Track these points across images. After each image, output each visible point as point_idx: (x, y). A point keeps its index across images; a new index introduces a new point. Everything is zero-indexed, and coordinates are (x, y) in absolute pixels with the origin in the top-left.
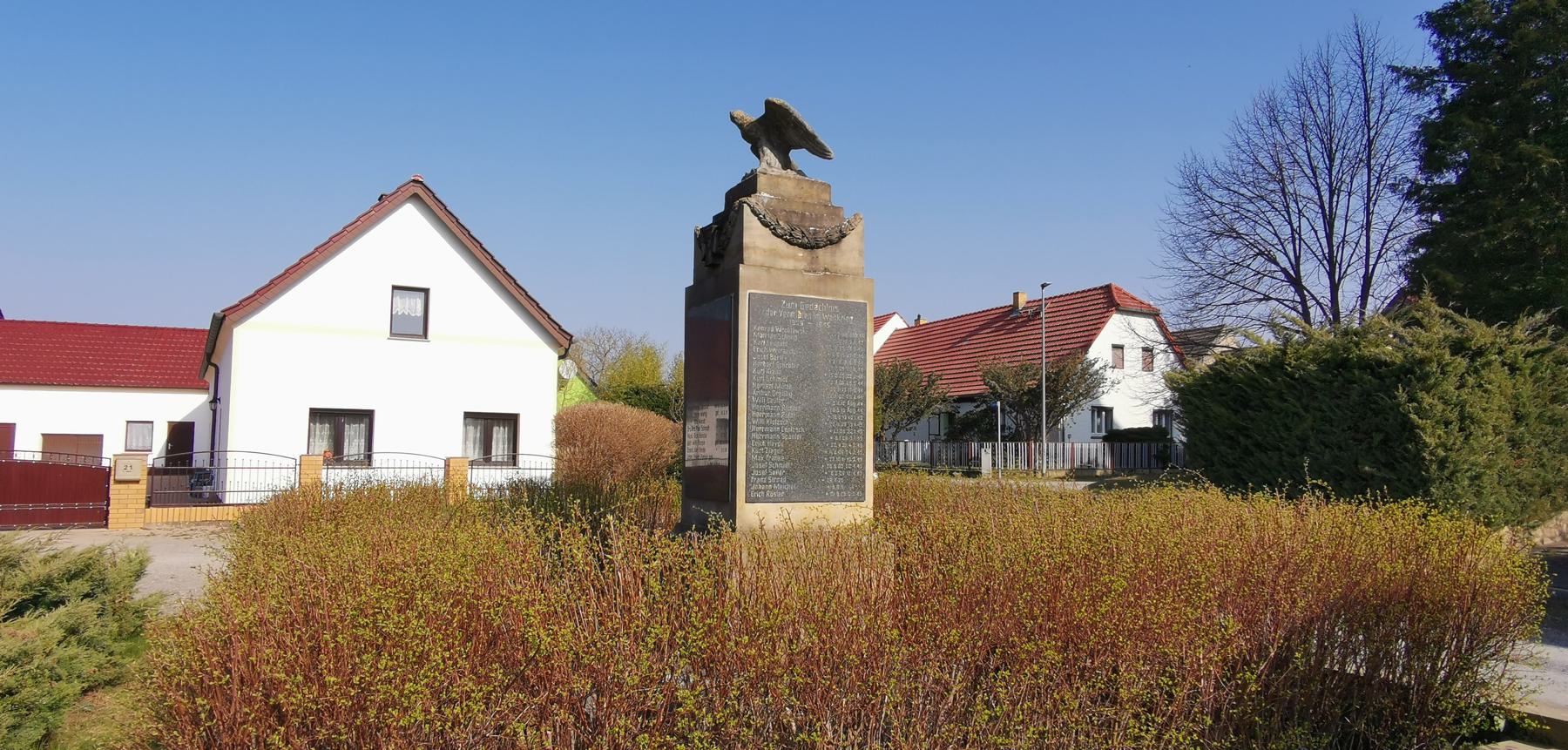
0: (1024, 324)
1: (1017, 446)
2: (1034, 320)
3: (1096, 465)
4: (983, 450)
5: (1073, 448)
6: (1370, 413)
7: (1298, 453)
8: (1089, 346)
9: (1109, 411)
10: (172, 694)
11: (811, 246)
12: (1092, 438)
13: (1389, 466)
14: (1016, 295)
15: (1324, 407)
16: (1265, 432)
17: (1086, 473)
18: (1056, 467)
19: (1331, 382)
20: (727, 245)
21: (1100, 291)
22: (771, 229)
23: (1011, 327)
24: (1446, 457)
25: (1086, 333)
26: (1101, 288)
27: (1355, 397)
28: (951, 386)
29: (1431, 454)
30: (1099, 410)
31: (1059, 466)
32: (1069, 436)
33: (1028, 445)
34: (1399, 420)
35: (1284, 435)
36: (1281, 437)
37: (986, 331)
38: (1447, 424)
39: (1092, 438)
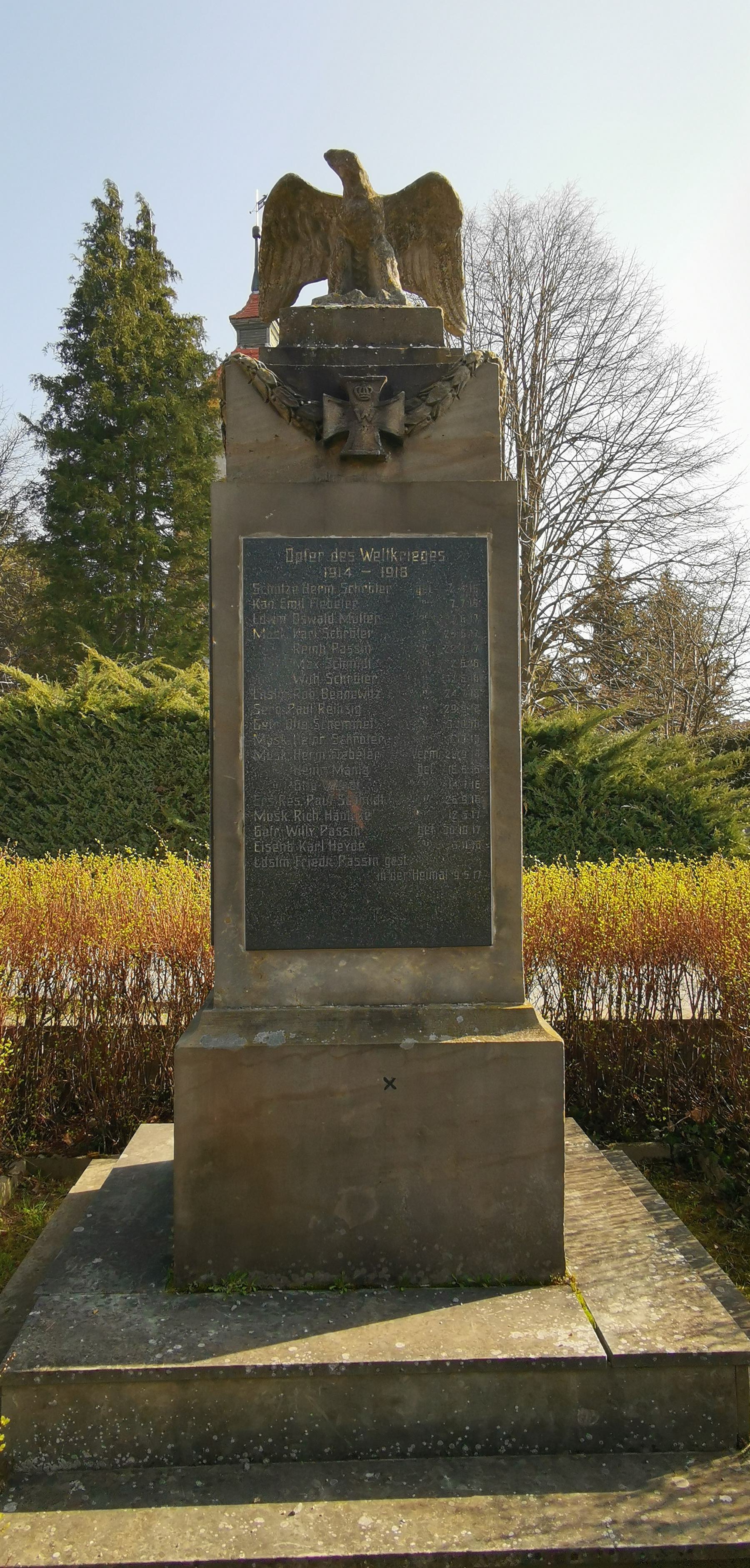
6: (173, 766)
13: (190, 818)
15: (127, 759)
20: (424, 429)
36: (67, 789)
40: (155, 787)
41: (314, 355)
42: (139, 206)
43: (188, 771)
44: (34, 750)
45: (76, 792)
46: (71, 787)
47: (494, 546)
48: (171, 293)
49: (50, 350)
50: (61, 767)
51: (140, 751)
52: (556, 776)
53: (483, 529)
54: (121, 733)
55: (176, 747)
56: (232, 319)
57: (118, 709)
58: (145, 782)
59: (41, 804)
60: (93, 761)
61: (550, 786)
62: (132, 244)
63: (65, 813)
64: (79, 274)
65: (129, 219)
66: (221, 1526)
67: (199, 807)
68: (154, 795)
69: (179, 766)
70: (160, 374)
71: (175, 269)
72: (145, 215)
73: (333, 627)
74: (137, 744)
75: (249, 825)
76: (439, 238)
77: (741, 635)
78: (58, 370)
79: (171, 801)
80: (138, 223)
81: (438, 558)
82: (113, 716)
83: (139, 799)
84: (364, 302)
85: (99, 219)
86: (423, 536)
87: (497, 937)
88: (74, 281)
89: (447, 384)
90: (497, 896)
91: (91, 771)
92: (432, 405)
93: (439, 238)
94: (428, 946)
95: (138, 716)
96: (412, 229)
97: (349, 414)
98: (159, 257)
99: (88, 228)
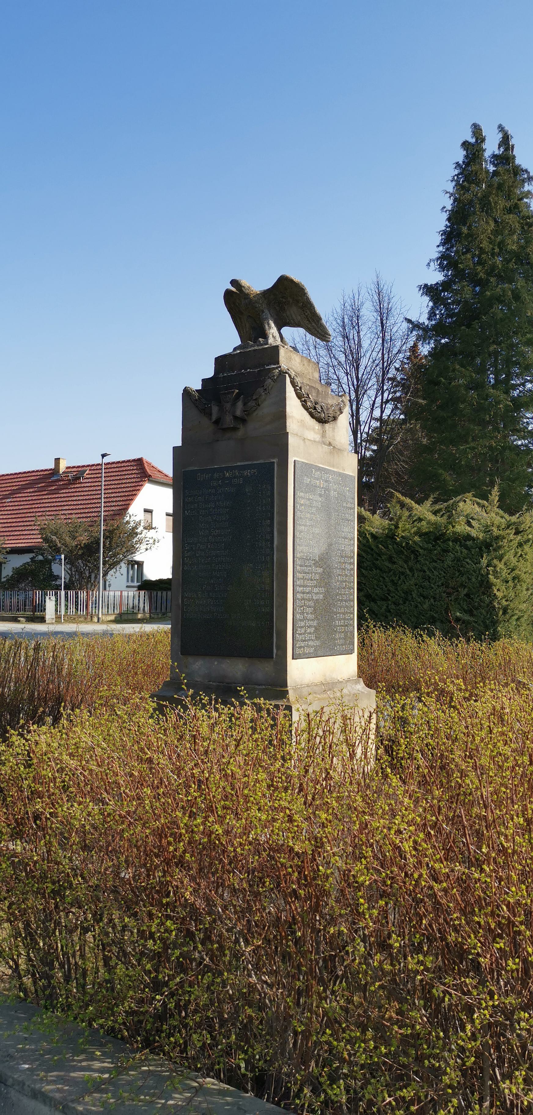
0: (65, 486)
1: (77, 594)
2: (74, 484)
3: (139, 610)
4: (47, 598)
5: (121, 596)
6: (457, 574)
7: (401, 602)
8: (127, 509)
9: (140, 565)
10: (425, 606)
11: (322, 421)
12: (127, 587)
13: (470, 612)
14: (57, 461)
15: (425, 568)
16: (376, 587)
17: (130, 617)
18: (108, 612)
19: (431, 550)
21: (133, 463)
23: (53, 488)
24: (508, 605)
25: (125, 498)
26: (134, 460)
27: (448, 562)
28: (6, 538)
29: (499, 603)
30: (133, 563)
31: (111, 611)
32: (110, 586)
33: (87, 592)
34: (479, 579)
35: (392, 589)
36: (389, 590)
37: (28, 491)
38: (507, 582)
39: (127, 587)
40: (445, 589)
41: (222, 379)
42: (500, 135)
44: (369, 563)
45: (395, 592)
46: (391, 589)
47: (278, 465)
49: (432, 264)
50: (384, 575)
53: (274, 458)
54: (420, 550)
57: (419, 533)
59: (374, 600)
60: (403, 570)
62: (495, 165)
63: (387, 607)
64: (449, 204)
66: (164, 902)
67: (476, 604)
68: (444, 595)
69: (462, 574)
70: (512, 265)
72: (506, 141)
73: (214, 508)
74: (432, 558)
75: (183, 598)
76: (298, 301)
79: (456, 599)
80: (499, 148)
81: (255, 473)
82: (417, 538)
83: (434, 598)
84: (252, 346)
85: (466, 157)
86: (250, 463)
87: (276, 655)
88: (445, 209)
89: (262, 388)
90: (277, 634)
91: (402, 577)
92: (256, 400)
93: (298, 301)
95: (432, 538)
96: (284, 300)
98: (517, 171)
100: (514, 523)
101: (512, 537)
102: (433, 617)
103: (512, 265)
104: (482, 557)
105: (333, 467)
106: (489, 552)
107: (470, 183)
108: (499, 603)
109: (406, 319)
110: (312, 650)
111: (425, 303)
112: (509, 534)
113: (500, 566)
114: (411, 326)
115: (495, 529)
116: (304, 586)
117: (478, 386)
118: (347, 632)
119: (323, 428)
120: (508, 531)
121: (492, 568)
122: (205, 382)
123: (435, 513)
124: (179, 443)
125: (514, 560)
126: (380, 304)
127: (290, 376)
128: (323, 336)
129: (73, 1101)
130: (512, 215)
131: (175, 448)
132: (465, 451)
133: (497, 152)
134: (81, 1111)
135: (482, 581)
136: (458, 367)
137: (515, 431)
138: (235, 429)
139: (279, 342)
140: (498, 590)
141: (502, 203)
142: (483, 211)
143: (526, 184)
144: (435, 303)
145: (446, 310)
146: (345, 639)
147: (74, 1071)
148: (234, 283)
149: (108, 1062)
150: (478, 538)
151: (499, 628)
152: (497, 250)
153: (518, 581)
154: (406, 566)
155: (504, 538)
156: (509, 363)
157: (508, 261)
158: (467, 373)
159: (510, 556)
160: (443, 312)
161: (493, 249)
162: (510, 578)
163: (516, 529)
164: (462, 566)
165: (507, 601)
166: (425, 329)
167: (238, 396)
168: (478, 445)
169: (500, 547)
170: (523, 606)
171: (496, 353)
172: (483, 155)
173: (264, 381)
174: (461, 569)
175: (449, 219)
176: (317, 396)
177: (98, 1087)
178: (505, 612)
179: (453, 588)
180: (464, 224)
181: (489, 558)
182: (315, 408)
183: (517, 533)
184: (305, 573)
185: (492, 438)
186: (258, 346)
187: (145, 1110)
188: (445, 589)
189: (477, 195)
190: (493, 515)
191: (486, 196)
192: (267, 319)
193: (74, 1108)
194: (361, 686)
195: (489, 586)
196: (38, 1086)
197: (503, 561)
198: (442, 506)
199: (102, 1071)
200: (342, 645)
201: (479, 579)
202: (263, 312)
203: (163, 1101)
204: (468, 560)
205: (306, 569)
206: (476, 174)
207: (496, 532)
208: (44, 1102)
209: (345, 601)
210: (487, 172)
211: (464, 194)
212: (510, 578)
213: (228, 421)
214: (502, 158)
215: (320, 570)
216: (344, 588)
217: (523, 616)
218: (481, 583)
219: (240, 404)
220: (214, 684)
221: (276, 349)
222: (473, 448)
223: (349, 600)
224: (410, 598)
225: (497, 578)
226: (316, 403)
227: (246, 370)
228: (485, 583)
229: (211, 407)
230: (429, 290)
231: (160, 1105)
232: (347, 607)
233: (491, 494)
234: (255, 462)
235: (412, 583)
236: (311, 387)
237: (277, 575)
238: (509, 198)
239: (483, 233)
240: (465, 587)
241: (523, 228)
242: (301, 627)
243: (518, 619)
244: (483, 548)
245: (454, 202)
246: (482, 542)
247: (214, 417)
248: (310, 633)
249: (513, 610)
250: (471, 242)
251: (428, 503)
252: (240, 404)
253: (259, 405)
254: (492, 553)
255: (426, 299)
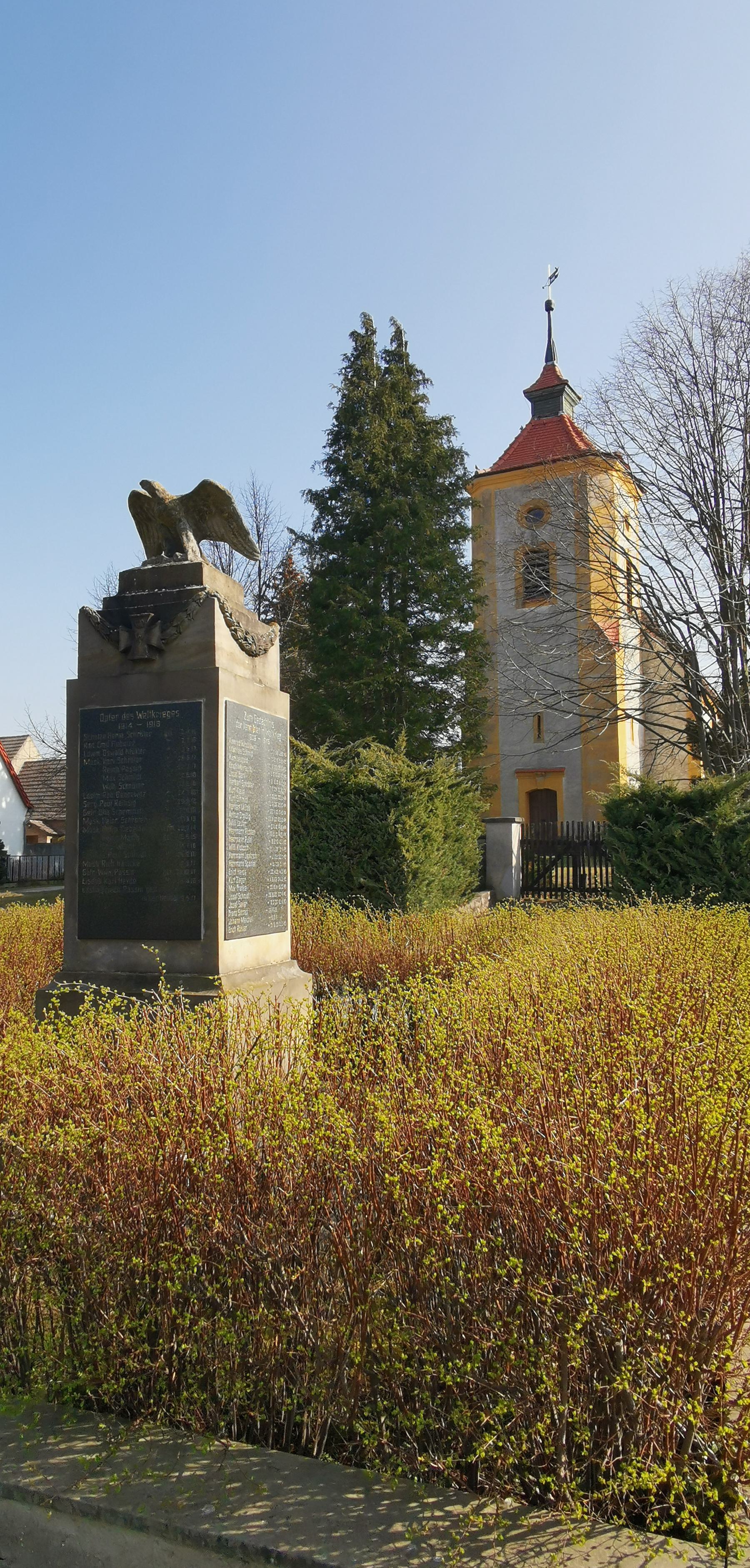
6: (360, 832)
10: (323, 872)
11: (252, 654)
19: (329, 804)
20: (175, 639)
22: (231, 630)
24: (418, 869)
27: (350, 818)
29: (408, 866)
34: (386, 838)
38: (417, 841)
42: (393, 329)
43: (373, 837)
47: (206, 705)
48: (424, 398)
49: (317, 466)
51: (333, 821)
52: (697, 838)
53: (201, 697)
55: (362, 816)
56: (525, 392)
57: (320, 786)
58: (338, 847)
61: (691, 848)
62: (387, 362)
64: (337, 400)
65: (383, 342)
67: (382, 868)
70: (408, 476)
71: (427, 377)
72: (398, 335)
75: (81, 868)
76: (222, 512)
77: (661, 716)
78: (323, 482)
79: (358, 863)
82: (312, 790)
83: (334, 862)
84: (167, 561)
85: (355, 349)
86: (170, 702)
87: (205, 935)
90: (205, 911)
92: (176, 626)
93: (222, 512)
94: (169, 940)
97: (132, 636)
98: (411, 371)
99: (346, 357)
100: (425, 773)
101: (422, 789)
102: (331, 884)
103: (408, 476)
104: (389, 813)
105: (265, 708)
106: (397, 806)
107: (360, 378)
108: (408, 866)
109: (288, 529)
110: (245, 929)
111: (310, 512)
112: (419, 786)
113: (410, 822)
114: (294, 537)
115: (403, 780)
116: (236, 852)
117: (373, 612)
118: (280, 906)
119: (253, 662)
120: (418, 782)
121: (400, 825)
122: (107, 601)
123: (332, 759)
124: (75, 676)
125: (424, 816)
126: (256, 508)
127: (219, 600)
128: (251, 553)
129: (65, 1491)
130: (406, 420)
131: (69, 683)
132: (358, 688)
133: (389, 348)
134: (77, 1502)
135: (389, 841)
136: (349, 588)
137: (415, 666)
138: (149, 661)
139: (200, 560)
140: (408, 851)
141: (395, 406)
142: (374, 412)
143: (421, 387)
144: (321, 513)
145: (334, 521)
146: (278, 914)
147: (53, 1457)
148: (145, 484)
149: (92, 1440)
150: (384, 790)
151: (408, 896)
152: (391, 458)
153: (429, 841)
154: (299, 823)
155: (414, 791)
156: (405, 588)
157: (404, 471)
158: (360, 596)
159: (421, 812)
160: (330, 523)
161: (387, 456)
162: (420, 837)
163: (427, 780)
164: (365, 823)
165: (416, 863)
166: (311, 542)
167: (154, 621)
168: (373, 680)
169: (409, 801)
170: (435, 869)
171: (391, 576)
172: (373, 349)
173: (187, 604)
174: (365, 826)
175: (337, 418)
176: (247, 625)
177: (93, 1470)
178: (415, 876)
179: (355, 850)
180: (354, 424)
181: (397, 813)
182: (246, 639)
183: (428, 784)
184: (237, 836)
185: (389, 673)
186: (175, 561)
187: (158, 1488)
188: (345, 851)
189: (368, 392)
190: (400, 762)
191: (378, 396)
192: (185, 529)
193: (68, 1499)
194: (295, 969)
195: (397, 846)
196: (12, 1481)
197: (412, 818)
198: (338, 752)
199: (89, 1450)
200: (276, 921)
201: (386, 838)
202: (180, 521)
203: (177, 1474)
204: (373, 816)
205: (239, 831)
206: (366, 369)
207: (404, 783)
208: (24, 1500)
209: (278, 868)
210: (379, 368)
211: (354, 390)
212: (420, 837)
213: (142, 650)
214: (396, 355)
215: (253, 832)
216: (277, 853)
217: (434, 881)
218: (388, 843)
219: (156, 632)
220: (123, 974)
221: (198, 567)
222: (368, 685)
223: (283, 867)
224: (304, 861)
225: (406, 836)
226: (247, 633)
227: (160, 589)
228: (392, 843)
229: (118, 632)
230: (315, 497)
231: (174, 1480)
232: (280, 875)
233: (397, 739)
234: (176, 702)
235: (307, 844)
236: (241, 613)
237: (205, 839)
238: (402, 399)
239: (376, 437)
240: (369, 848)
241: (419, 435)
242: (234, 901)
243: (428, 885)
244: (390, 802)
245: (342, 399)
246: (388, 796)
247: (123, 646)
248: (242, 908)
249: (423, 873)
250: (363, 445)
251: (324, 748)
252: (156, 632)
253: (180, 633)
254: (400, 807)
255: (312, 506)
